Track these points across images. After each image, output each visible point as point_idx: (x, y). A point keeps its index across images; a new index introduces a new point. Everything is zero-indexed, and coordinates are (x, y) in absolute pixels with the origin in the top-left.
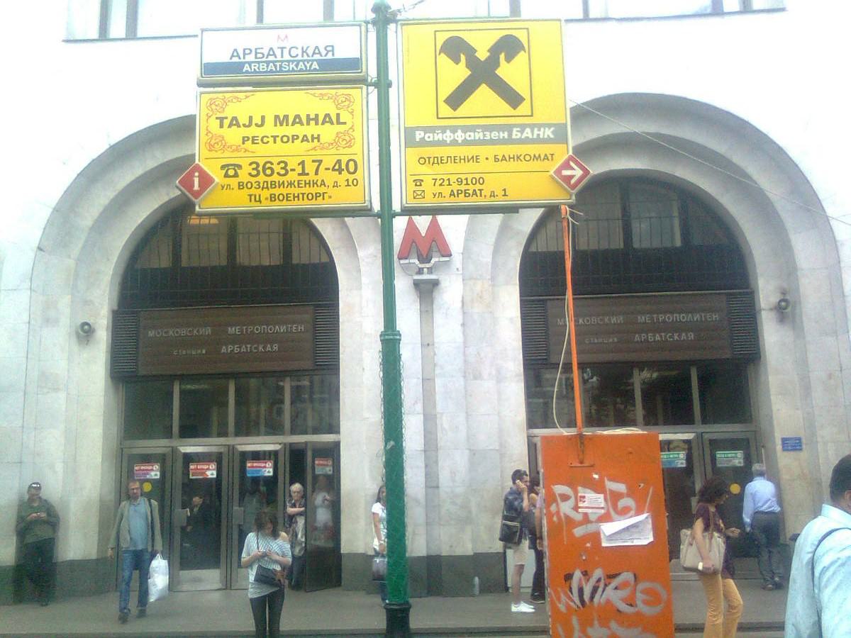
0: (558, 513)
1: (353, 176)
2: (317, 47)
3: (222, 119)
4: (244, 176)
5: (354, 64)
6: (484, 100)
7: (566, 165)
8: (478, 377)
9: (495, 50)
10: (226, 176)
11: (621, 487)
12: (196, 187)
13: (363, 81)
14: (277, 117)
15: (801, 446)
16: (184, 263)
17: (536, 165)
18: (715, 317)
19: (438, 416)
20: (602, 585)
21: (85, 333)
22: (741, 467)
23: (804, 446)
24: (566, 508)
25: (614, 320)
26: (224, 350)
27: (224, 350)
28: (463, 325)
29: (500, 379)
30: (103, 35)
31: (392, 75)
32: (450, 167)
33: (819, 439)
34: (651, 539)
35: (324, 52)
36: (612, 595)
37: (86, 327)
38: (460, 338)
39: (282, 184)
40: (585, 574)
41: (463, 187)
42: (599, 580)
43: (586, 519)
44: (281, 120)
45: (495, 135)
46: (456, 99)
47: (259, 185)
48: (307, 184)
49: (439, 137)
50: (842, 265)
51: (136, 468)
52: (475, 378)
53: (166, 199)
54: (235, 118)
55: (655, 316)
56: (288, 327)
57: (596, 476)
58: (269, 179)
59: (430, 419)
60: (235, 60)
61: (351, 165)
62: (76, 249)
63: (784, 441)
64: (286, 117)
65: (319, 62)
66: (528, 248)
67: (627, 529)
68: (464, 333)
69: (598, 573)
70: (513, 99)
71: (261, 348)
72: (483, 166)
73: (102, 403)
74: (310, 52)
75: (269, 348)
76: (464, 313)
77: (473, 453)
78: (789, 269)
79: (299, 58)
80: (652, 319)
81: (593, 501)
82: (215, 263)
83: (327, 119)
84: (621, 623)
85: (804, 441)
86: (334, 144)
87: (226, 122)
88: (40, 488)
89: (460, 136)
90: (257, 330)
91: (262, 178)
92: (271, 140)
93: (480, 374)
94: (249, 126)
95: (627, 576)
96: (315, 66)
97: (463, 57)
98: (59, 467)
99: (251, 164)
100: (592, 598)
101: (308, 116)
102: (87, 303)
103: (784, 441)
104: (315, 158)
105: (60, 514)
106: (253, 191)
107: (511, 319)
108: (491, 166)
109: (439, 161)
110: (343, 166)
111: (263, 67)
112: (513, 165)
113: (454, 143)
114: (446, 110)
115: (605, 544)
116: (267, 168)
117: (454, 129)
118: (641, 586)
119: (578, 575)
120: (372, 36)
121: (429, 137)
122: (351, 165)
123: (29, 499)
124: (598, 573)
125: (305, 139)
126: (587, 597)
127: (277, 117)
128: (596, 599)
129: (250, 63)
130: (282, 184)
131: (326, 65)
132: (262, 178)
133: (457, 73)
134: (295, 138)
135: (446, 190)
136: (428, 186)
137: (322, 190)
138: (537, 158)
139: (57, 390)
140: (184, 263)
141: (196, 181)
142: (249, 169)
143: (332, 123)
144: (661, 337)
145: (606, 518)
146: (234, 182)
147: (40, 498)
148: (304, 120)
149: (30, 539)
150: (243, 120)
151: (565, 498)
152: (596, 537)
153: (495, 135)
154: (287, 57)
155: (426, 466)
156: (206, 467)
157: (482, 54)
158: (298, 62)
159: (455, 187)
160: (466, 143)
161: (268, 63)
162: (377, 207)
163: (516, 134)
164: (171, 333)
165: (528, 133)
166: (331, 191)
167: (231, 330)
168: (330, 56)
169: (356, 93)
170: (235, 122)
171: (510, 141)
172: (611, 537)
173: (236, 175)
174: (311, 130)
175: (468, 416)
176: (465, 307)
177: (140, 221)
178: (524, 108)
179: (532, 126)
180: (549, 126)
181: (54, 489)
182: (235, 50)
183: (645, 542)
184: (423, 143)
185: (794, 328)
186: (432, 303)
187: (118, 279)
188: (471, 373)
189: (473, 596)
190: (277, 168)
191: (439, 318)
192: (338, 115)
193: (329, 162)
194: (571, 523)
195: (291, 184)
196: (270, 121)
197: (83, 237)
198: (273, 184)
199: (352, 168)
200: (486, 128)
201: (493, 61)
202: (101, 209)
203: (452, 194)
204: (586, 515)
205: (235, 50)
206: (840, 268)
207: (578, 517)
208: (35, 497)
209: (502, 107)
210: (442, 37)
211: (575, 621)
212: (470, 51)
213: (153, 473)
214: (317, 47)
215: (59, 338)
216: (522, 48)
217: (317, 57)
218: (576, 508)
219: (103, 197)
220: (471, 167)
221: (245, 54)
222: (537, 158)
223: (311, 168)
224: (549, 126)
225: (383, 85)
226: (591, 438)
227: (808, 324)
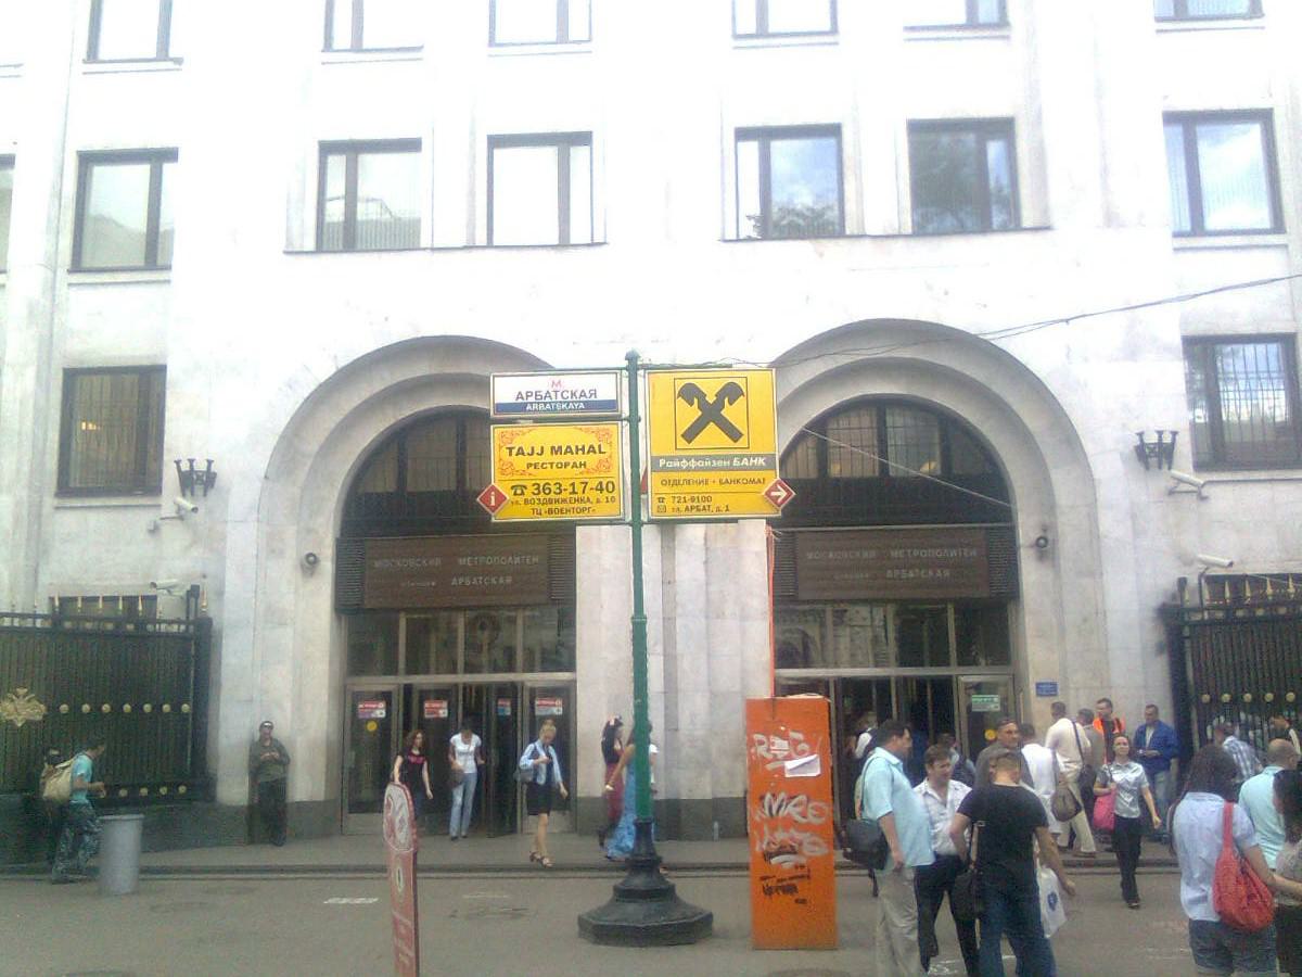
0: (756, 753)
1: (611, 495)
2: (583, 391)
3: (510, 449)
4: (528, 494)
5: (612, 405)
6: (712, 436)
7: (774, 488)
8: (721, 615)
9: (721, 395)
10: (515, 494)
11: (799, 736)
12: (493, 503)
13: (619, 418)
14: (553, 448)
15: (1056, 691)
16: (410, 488)
17: (751, 487)
18: (974, 553)
19: (679, 658)
20: (784, 804)
21: (310, 563)
22: (996, 713)
23: (1059, 691)
24: (761, 750)
25: (866, 555)
26: (454, 582)
27: (454, 582)
28: (706, 562)
29: (744, 617)
31: (641, 413)
32: (686, 488)
33: (1072, 686)
34: (818, 772)
35: (588, 395)
36: (791, 810)
37: (312, 558)
38: (701, 574)
39: (557, 501)
40: (774, 795)
41: (695, 504)
42: (783, 801)
43: (775, 758)
44: (556, 450)
45: (720, 463)
46: (690, 435)
47: (538, 489)
48: (577, 500)
49: (677, 464)
50: (1099, 504)
51: (361, 706)
52: (718, 617)
53: (393, 421)
54: (520, 448)
55: (909, 551)
56: (906, 553)
57: (782, 728)
58: (548, 497)
59: (670, 658)
60: (520, 401)
61: (610, 486)
62: (301, 475)
63: (1038, 685)
64: (560, 448)
65: (584, 402)
67: (803, 765)
68: (706, 571)
69: (782, 795)
70: (734, 434)
71: (931, 573)
72: (711, 488)
74: (578, 395)
76: (707, 549)
77: (713, 695)
78: (1049, 506)
79: (569, 399)
81: (780, 745)
82: (444, 487)
83: (592, 449)
84: (797, 830)
85: (1059, 687)
86: (597, 469)
87: (515, 451)
88: (271, 727)
89: (693, 463)
91: (542, 496)
92: (549, 466)
93: (723, 613)
94: (532, 454)
95: (802, 798)
96: (582, 406)
97: (696, 400)
98: (288, 705)
99: (534, 485)
100: (778, 811)
101: (577, 447)
102: (309, 531)
103: (1038, 685)
104: (582, 480)
105: (291, 756)
106: (536, 506)
107: (757, 554)
108: (717, 487)
109: (676, 483)
110: (604, 486)
111: (541, 407)
112: (734, 487)
113: (688, 469)
114: (682, 443)
115: (787, 776)
116: (546, 489)
117: (688, 459)
118: (810, 805)
119: (768, 796)
120: (626, 382)
121: (670, 464)
122: (610, 486)
123: (261, 737)
124: (782, 795)
125: (575, 465)
126: (774, 812)
127: (553, 448)
128: (781, 813)
129: (531, 403)
130: (557, 501)
131: (589, 405)
132: (542, 496)
133: (692, 413)
134: (566, 465)
135: (683, 506)
136: (669, 503)
137: (588, 505)
138: (753, 481)
139: (282, 624)
140: (410, 488)
141: (493, 498)
142: (533, 489)
143: (595, 452)
145: (788, 758)
146: (521, 499)
147: (271, 739)
148: (574, 449)
149: (262, 779)
150: (527, 450)
151: (761, 743)
152: (781, 770)
153: (720, 463)
154: (559, 399)
155: (666, 708)
156: (438, 705)
157: (711, 399)
158: (568, 403)
159: (689, 504)
160: (697, 469)
161: (545, 404)
162: (629, 518)
163: (736, 463)
165: (745, 462)
166: (595, 506)
167: (462, 561)
168: (593, 398)
169: (612, 427)
170: (521, 452)
171: (731, 469)
172: (792, 770)
173: (523, 493)
174: (580, 458)
175: (709, 655)
176: (709, 543)
177: (366, 444)
178: (742, 442)
179: (748, 457)
180: (762, 456)
181: (283, 730)
182: (520, 393)
183: (814, 774)
184: (665, 469)
185: (1054, 566)
186: (674, 540)
187: (341, 505)
188: (713, 611)
189: (712, 839)
190: (553, 488)
191: (680, 555)
192: (600, 446)
193: (593, 483)
194: (765, 761)
195: (564, 501)
196: (547, 451)
197: (309, 463)
198: (550, 501)
199: (610, 489)
200: (712, 458)
201: (719, 404)
202: (326, 434)
203: (687, 508)
204: (775, 755)
205: (520, 393)
206: (1096, 507)
207: (769, 756)
208: (267, 737)
209: (725, 440)
210: (680, 384)
211: (766, 828)
212: (701, 396)
213: (378, 712)
214: (583, 391)
215: (285, 569)
216: (743, 394)
217: (583, 399)
218: (768, 750)
219: (330, 420)
220: (703, 488)
221: (527, 396)
222: (753, 481)
223: (579, 488)
224: (762, 456)
225: (634, 420)
226: (781, 702)
227: (1065, 563)
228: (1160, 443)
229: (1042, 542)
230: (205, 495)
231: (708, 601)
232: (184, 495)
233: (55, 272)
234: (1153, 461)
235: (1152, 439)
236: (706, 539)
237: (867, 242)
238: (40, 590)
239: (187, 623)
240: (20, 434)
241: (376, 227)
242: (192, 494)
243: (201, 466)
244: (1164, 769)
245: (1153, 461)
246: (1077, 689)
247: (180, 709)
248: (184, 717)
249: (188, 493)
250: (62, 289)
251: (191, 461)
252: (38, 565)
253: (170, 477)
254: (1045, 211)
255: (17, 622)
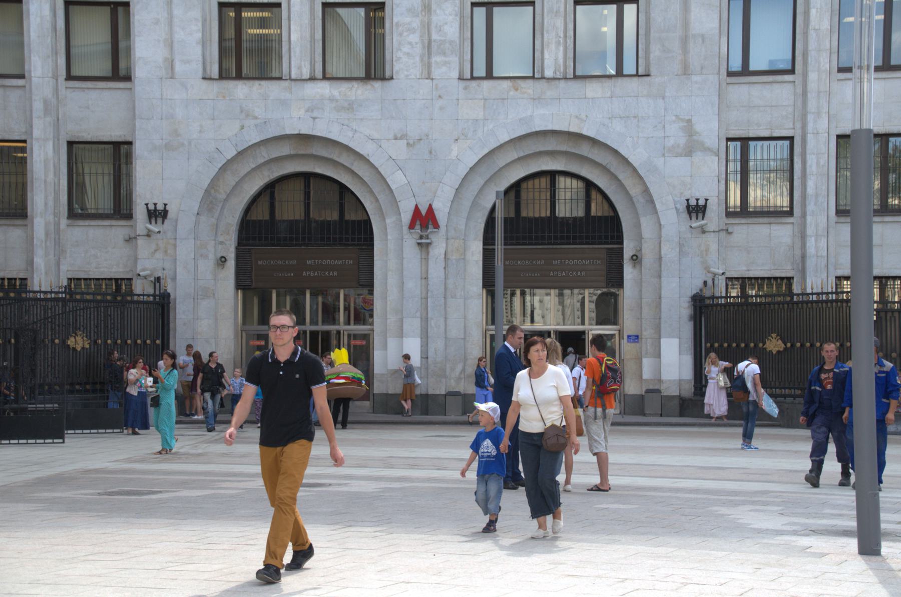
25: (291, 262)
26: (304, 274)
27: (304, 274)
28: (445, 268)
30: (620, 73)
37: (223, 259)
52: (452, 297)
56: (315, 262)
63: (629, 337)
66: (246, 217)
73: (233, 304)
75: (331, 274)
78: (639, 238)
80: (315, 262)
90: (571, 262)
103: (629, 337)
107: (477, 262)
144: (565, 273)
164: (272, 262)
167: (309, 262)
228: (697, 205)
229: (635, 258)
230: (163, 223)
231: (446, 289)
232: (151, 223)
233: (57, 80)
234: (694, 215)
235: (693, 202)
236: (445, 254)
237: (544, 80)
238: (61, 274)
239: (154, 295)
240: (45, 181)
241: (261, 38)
242: (156, 223)
243: (160, 207)
244: (683, 380)
245: (694, 215)
246: (646, 339)
247: (155, 343)
248: (158, 346)
249: (153, 221)
250: (63, 92)
251: (155, 204)
252: (59, 258)
253: (140, 213)
254: (648, 65)
255: (53, 295)
